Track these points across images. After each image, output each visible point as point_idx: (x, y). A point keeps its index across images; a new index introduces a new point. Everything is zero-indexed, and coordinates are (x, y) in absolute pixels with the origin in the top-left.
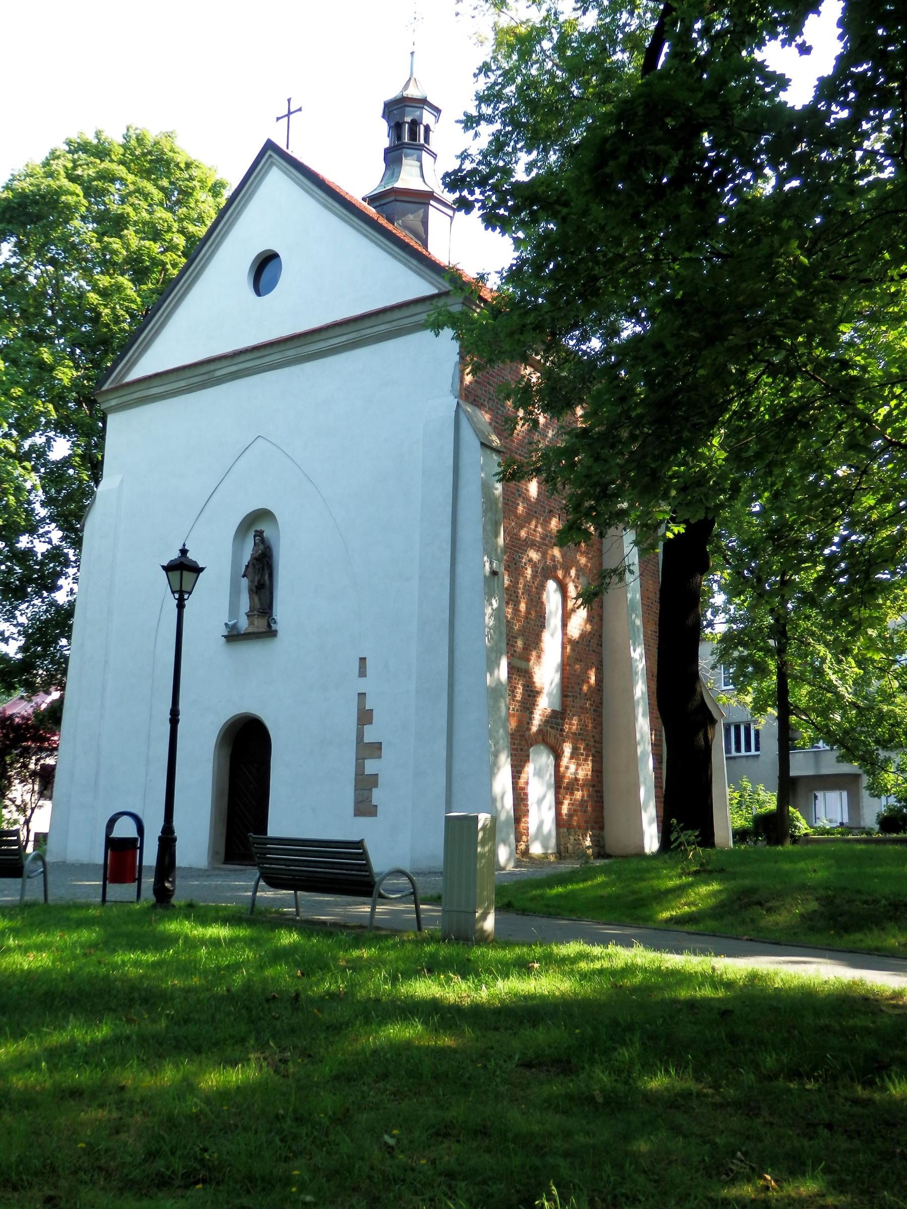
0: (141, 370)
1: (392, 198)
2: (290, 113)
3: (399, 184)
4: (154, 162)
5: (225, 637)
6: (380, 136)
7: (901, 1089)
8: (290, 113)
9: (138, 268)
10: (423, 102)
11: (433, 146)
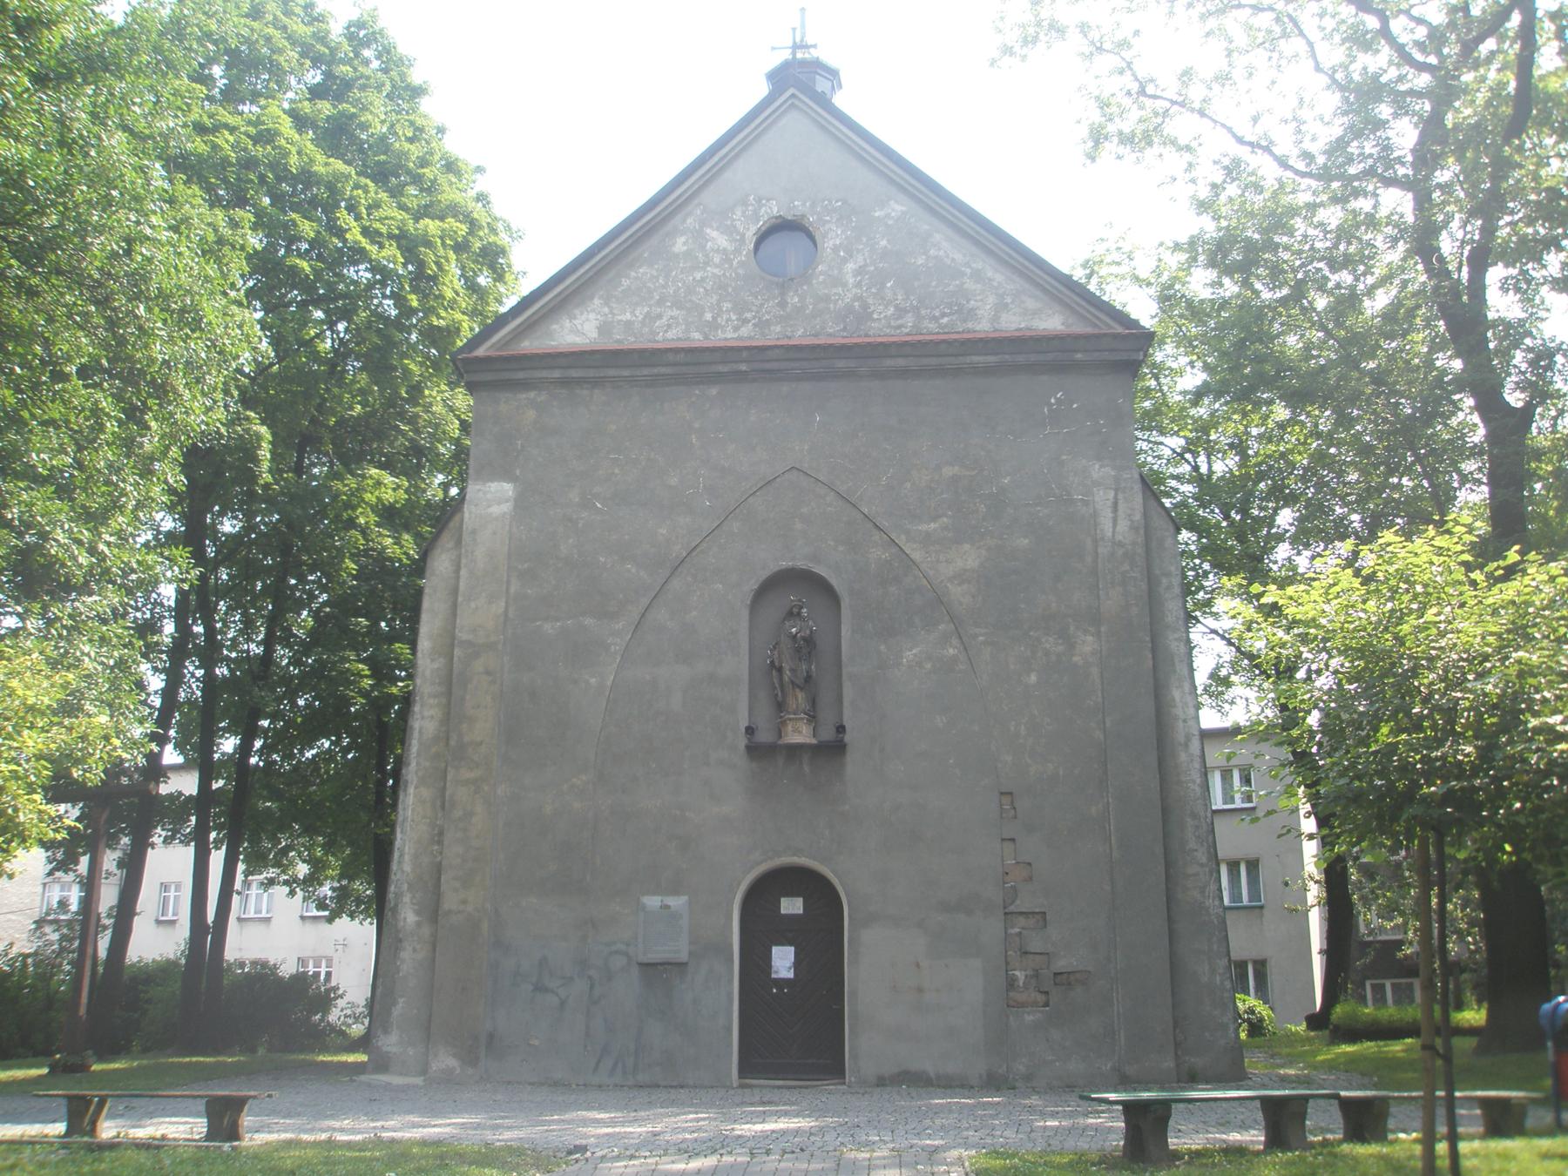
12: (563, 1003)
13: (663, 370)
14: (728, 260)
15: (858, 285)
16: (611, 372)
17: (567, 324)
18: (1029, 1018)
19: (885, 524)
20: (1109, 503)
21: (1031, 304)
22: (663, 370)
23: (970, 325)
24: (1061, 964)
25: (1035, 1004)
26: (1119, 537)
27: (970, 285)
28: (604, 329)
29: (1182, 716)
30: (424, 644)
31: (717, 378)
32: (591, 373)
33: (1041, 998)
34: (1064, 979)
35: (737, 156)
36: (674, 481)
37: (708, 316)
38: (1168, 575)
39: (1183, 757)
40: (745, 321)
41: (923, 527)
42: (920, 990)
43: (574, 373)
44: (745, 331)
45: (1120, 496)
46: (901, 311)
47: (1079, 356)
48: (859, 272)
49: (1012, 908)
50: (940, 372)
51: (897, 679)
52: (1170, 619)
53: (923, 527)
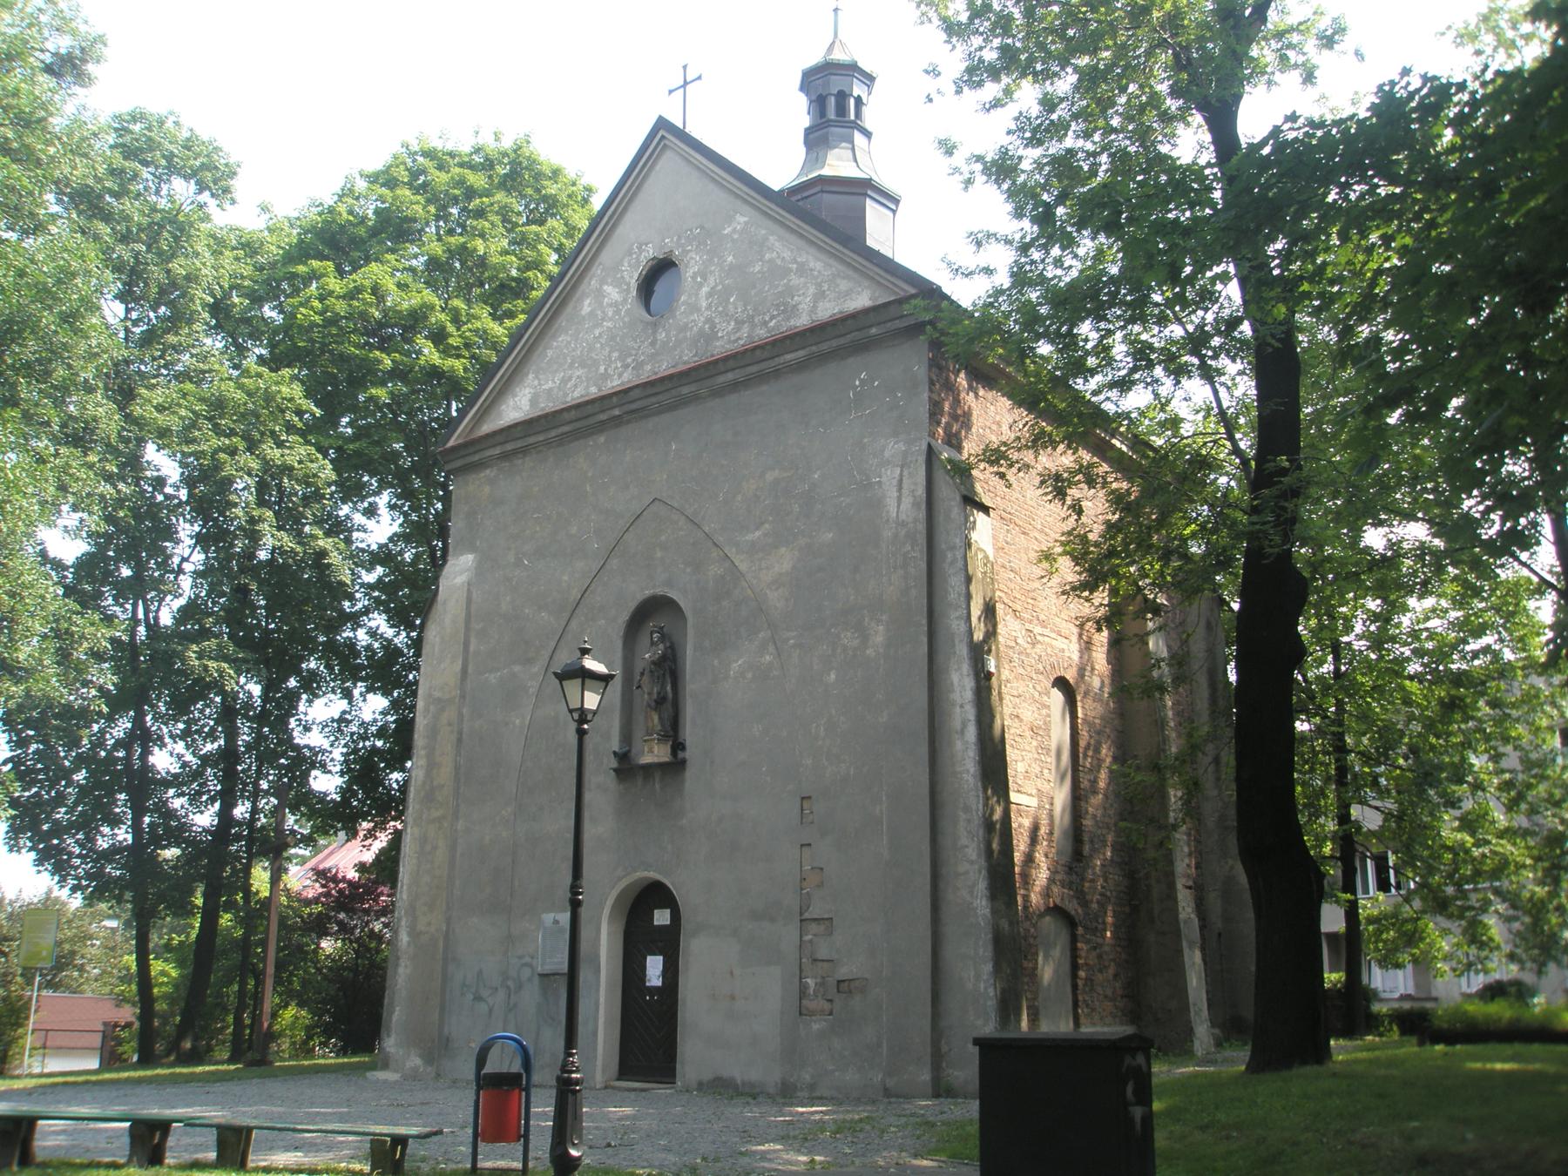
0: (517, 407)
1: (818, 189)
2: (686, 83)
3: (827, 171)
4: (518, 172)
5: (615, 770)
6: (798, 112)
7: (1563, 1088)
8: (686, 83)
9: (504, 293)
10: (852, 69)
11: (869, 121)
12: (491, 1011)
13: (566, 429)
14: (618, 312)
15: (709, 307)
16: (532, 440)
17: (511, 403)
18: (815, 1027)
19: (720, 539)
20: (895, 482)
21: (844, 285)
22: (566, 429)
23: (792, 323)
24: (843, 972)
25: (822, 1012)
26: (903, 517)
27: (795, 280)
28: (534, 401)
29: (959, 701)
30: (420, 704)
31: (602, 427)
32: (519, 444)
33: (827, 1006)
34: (844, 986)
35: (625, 209)
36: (574, 530)
37: (602, 369)
38: (953, 548)
39: (959, 745)
40: (626, 366)
41: (750, 537)
42: (733, 998)
43: (509, 447)
44: (626, 376)
45: (905, 473)
46: (739, 323)
47: (874, 331)
48: (710, 295)
49: (806, 915)
50: (762, 378)
51: (727, 687)
52: (952, 596)
53: (750, 537)
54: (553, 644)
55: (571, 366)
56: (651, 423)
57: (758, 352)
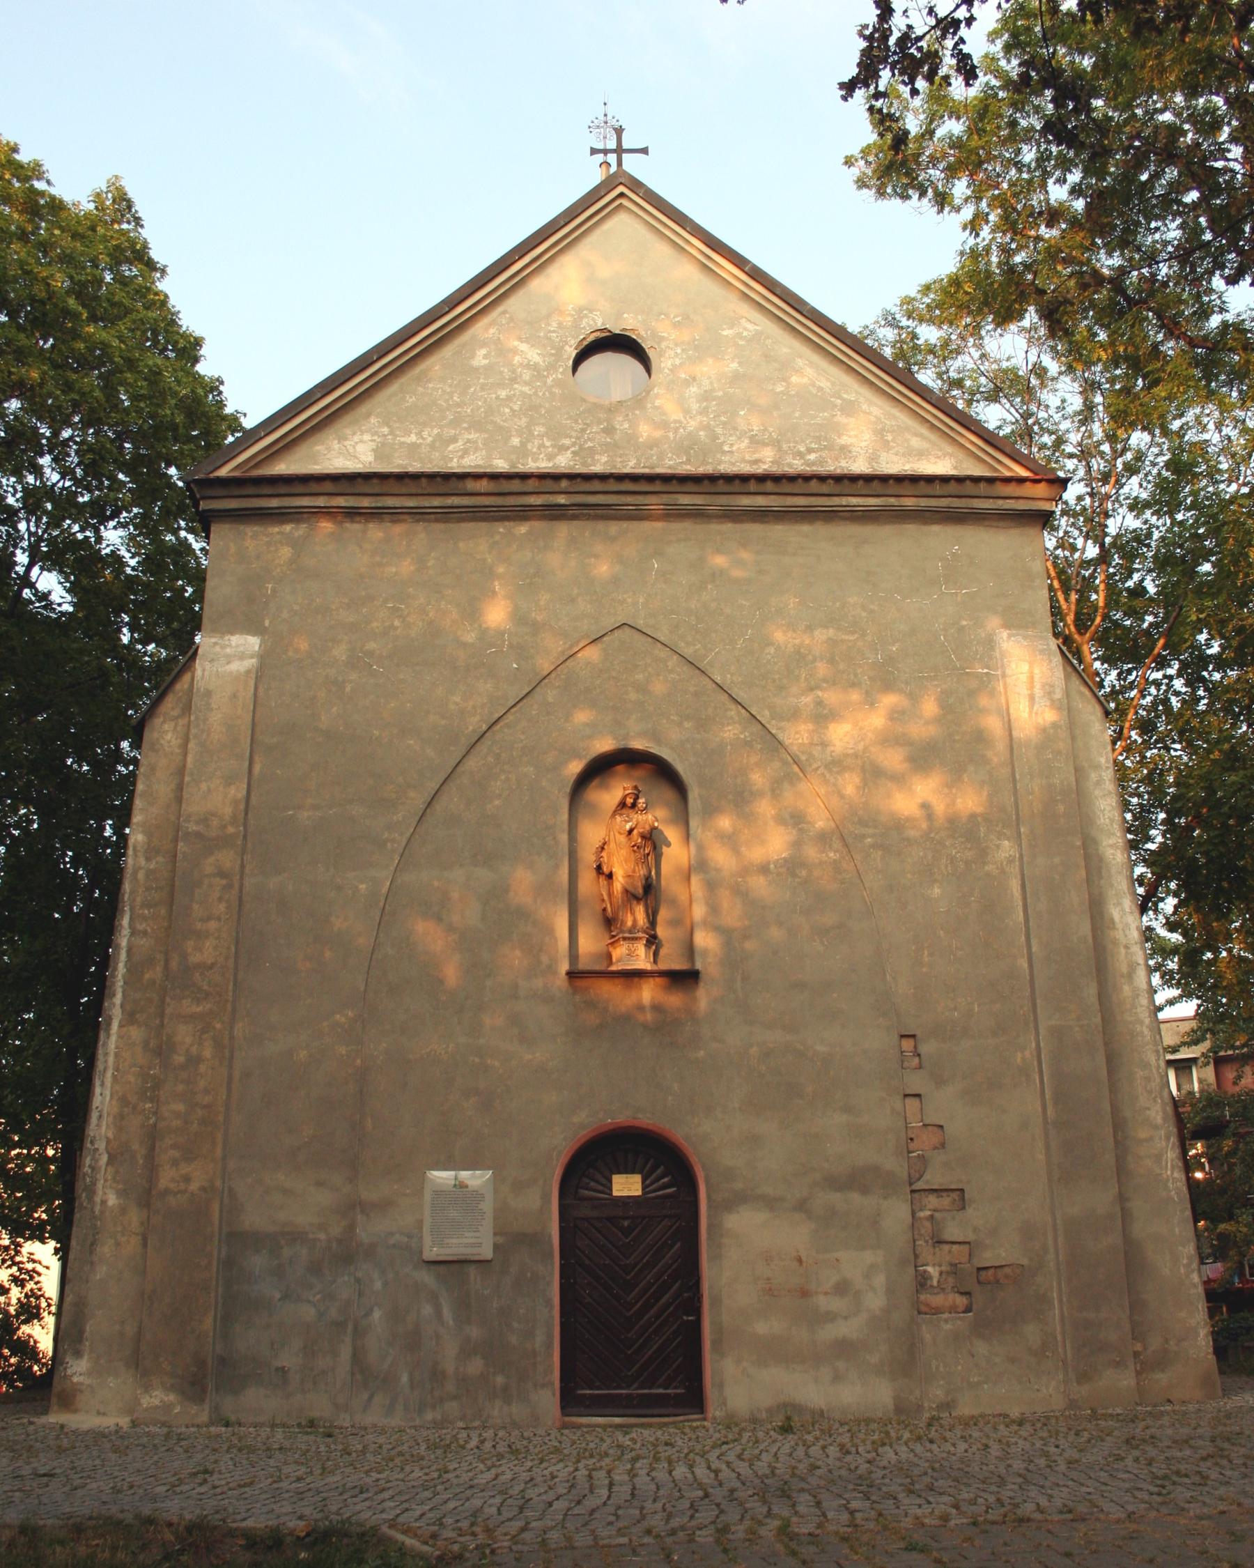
23: (843, 464)
24: (988, 1257)
25: (953, 1309)
29: (1123, 940)
33: (961, 1301)
37: (516, 441)
54: (434, 785)
55: (456, 422)
56: (614, 527)
57: (814, 483)
